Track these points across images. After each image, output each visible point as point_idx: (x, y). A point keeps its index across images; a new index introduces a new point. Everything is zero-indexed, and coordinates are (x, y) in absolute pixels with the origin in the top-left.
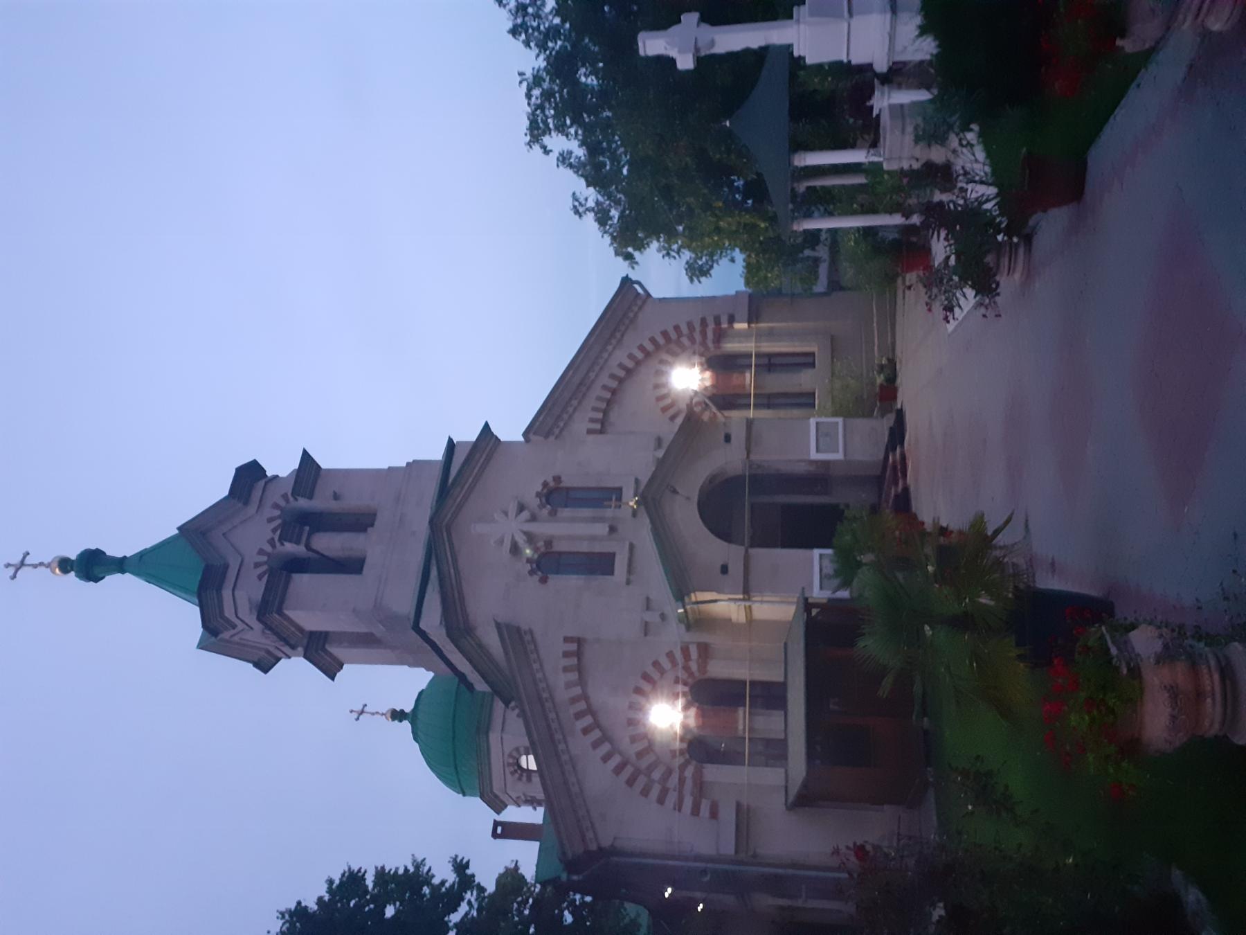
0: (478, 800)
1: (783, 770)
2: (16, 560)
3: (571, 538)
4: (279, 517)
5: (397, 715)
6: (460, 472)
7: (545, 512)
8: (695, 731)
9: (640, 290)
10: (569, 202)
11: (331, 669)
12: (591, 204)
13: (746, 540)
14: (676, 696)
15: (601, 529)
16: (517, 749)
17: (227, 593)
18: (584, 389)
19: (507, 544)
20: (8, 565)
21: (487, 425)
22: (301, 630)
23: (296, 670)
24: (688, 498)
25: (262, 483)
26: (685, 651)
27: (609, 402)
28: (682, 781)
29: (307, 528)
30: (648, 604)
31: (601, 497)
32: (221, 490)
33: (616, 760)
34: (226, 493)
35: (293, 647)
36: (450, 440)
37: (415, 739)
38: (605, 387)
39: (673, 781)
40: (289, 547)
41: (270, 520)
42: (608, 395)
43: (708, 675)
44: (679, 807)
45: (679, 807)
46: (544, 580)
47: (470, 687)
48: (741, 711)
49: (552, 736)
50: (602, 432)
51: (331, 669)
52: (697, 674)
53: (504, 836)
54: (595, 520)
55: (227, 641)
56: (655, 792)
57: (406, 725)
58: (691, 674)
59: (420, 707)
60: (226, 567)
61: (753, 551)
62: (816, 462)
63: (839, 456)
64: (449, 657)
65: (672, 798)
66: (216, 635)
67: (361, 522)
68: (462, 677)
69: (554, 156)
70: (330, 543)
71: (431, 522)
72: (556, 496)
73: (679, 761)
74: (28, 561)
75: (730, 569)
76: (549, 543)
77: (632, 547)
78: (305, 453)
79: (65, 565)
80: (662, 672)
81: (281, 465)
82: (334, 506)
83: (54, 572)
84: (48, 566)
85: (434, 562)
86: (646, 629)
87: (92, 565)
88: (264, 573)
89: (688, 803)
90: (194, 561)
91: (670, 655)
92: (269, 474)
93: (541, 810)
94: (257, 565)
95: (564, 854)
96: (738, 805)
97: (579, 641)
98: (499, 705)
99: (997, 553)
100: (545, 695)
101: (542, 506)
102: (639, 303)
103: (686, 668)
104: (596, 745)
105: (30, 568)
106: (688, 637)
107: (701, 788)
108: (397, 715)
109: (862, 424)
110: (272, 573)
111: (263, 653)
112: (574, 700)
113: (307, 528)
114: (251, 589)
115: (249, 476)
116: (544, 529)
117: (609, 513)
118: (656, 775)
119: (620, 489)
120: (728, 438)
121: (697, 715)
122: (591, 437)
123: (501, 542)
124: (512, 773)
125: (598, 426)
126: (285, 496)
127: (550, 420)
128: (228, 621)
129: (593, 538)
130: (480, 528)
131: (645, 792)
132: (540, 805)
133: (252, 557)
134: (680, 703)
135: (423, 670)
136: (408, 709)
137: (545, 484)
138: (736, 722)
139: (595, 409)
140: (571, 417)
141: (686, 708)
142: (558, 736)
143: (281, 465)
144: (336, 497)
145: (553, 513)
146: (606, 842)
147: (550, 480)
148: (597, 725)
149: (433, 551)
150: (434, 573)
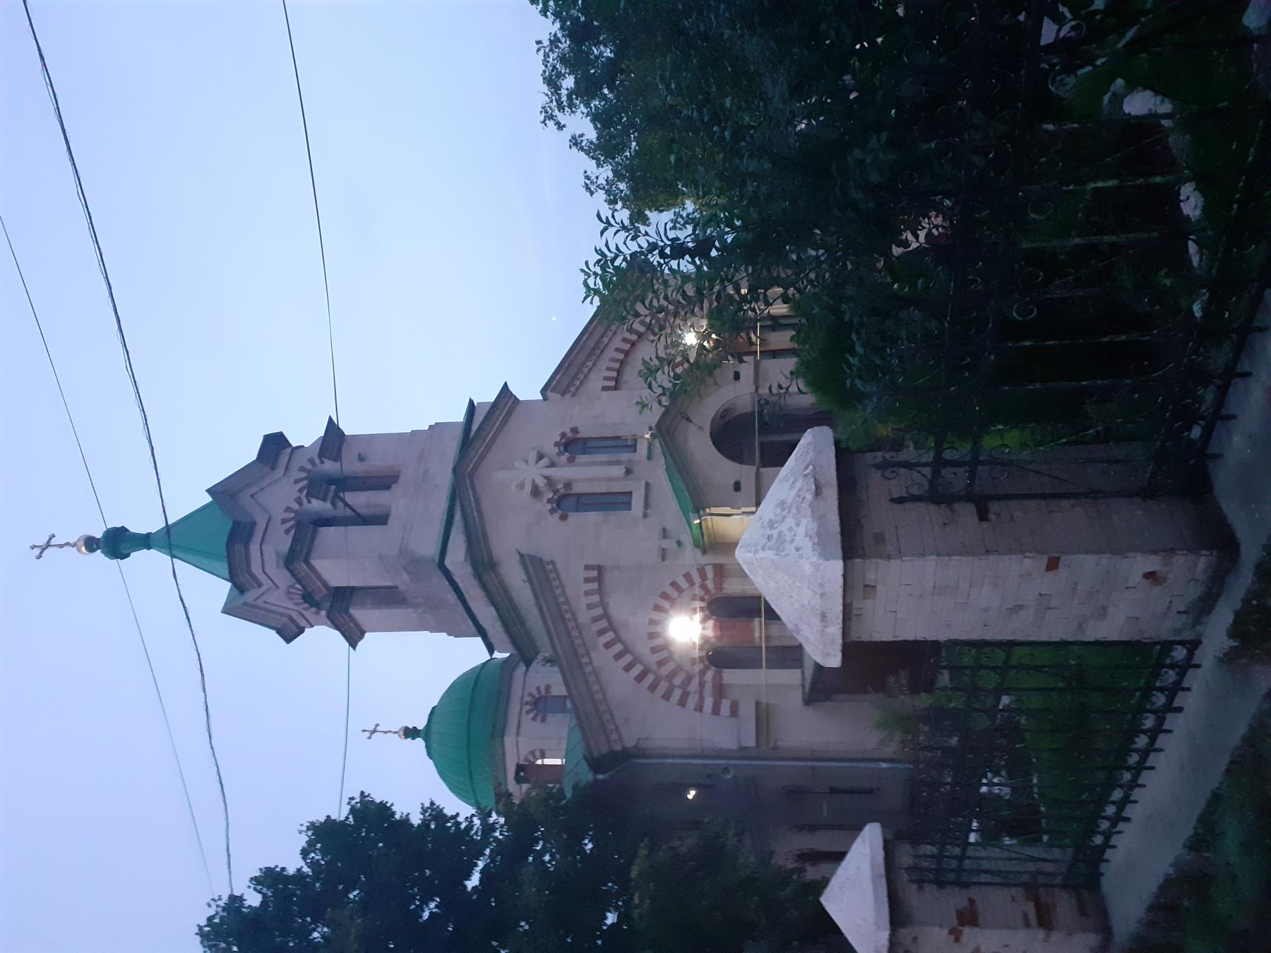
1: (799, 671)
2: (43, 542)
5: (410, 733)
6: (483, 423)
7: (564, 458)
8: (713, 640)
10: (582, 180)
11: (353, 636)
12: (602, 181)
13: (757, 459)
14: (694, 611)
15: (619, 471)
16: (533, 753)
17: (254, 548)
18: (598, 352)
19: (528, 488)
20: (33, 547)
21: (506, 384)
22: (325, 584)
23: (322, 638)
24: (701, 428)
25: (289, 450)
27: (622, 363)
28: (702, 684)
29: (333, 487)
30: (665, 534)
31: (621, 444)
32: (249, 453)
33: (638, 669)
34: (253, 456)
36: (471, 402)
37: (430, 754)
39: (696, 681)
41: (297, 482)
42: (621, 356)
44: (699, 708)
45: (699, 708)
46: (564, 518)
48: (756, 621)
49: (575, 651)
50: (616, 388)
52: (713, 591)
54: (611, 463)
56: (677, 694)
57: (420, 742)
58: (707, 591)
59: (434, 719)
60: (253, 525)
61: (763, 470)
65: (692, 701)
67: (385, 481)
69: (566, 135)
70: (359, 500)
71: (454, 470)
72: (573, 445)
73: (698, 667)
74: (53, 542)
76: (568, 485)
77: (647, 485)
79: (91, 544)
80: (680, 590)
81: (305, 434)
83: (79, 550)
84: (74, 545)
86: (664, 554)
87: (117, 543)
88: (291, 528)
89: (709, 702)
91: (688, 577)
94: (284, 521)
96: (758, 704)
97: (599, 569)
100: (568, 616)
101: (560, 454)
103: (703, 587)
104: (618, 657)
105: (55, 549)
106: (704, 560)
107: (720, 691)
108: (410, 733)
110: (299, 526)
111: (285, 619)
112: (596, 619)
115: (274, 445)
116: (563, 473)
118: (677, 681)
120: (737, 376)
121: (715, 626)
122: (606, 393)
123: (521, 486)
125: (613, 384)
126: (311, 461)
127: (566, 379)
129: (610, 479)
130: (502, 475)
131: (667, 696)
133: (279, 513)
134: (698, 617)
135: (445, 634)
136: (421, 726)
137: (563, 435)
138: (753, 630)
140: (586, 376)
141: (704, 621)
142: (581, 651)
143: (305, 434)
144: (361, 459)
146: (630, 742)
147: (567, 431)
148: (618, 639)
149: (455, 495)
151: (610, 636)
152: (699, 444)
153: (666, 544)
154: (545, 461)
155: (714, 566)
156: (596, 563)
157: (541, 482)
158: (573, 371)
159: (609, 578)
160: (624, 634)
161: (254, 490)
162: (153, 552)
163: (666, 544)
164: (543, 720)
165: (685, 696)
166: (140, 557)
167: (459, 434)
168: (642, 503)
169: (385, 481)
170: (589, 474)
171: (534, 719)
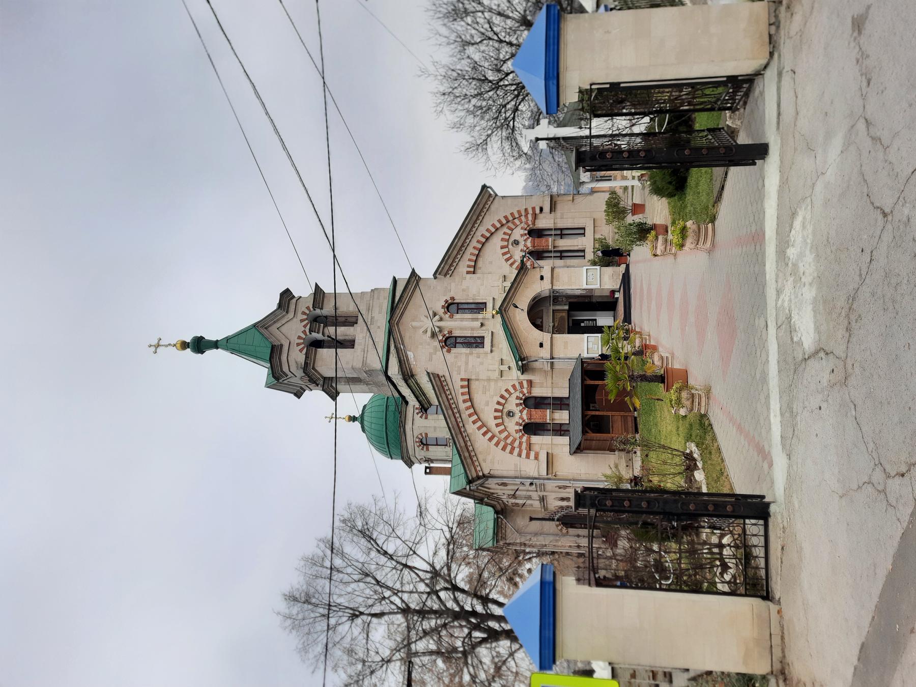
0: (401, 461)
2: (155, 342)
3: (461, 329)
5: (353, 419)
19: (429, 333)
20: (150, 346)
23: (316, 397)
25: (294, 301)
26: (521, 384)
27: (477, 256)
28: (521, 444)
33: (490, 435)
36: (394, 278)
38: (474, 248)
39: (516, 444)
41: (302, 321)
44: (520, 455)
45: (520, 455)
50: (474, 273)
53: (430, 473)
57: (357, 424)
60: (282, 345)
63: (598, 286)
65: (516, 451)
66: (277, 379)
67: (350, 321)
72: (453, 307)
77: (492, 333)
79: (184, 345)
81: (303, 291)
87: (199, 345)
88: (303, 348)
90: (257, 343)
94: (298, 344)
95: (468, 477)
99: (528, 166)
102: (491, 199)
108: (353, 419)
109: (609, 270)
112: (467, 408)
117: (480, 316)
118: (509, 441)
123: (426, 332)
125: (472, 269)
126: (308, 308)
128: (284, 373)
129: (473, 329)
137: (446, 301)
139: (470, 260)
143: (303, 291)
145: (451, 317)
148: (479, 419)
149: (390, 333)
151: (475, 417)
152: (521, 319)
153: (502, 368)
154: (437, 317)
156: (467, 377)
158: (450, 261)
159: (474, 385)
160: (481, 416)
161: (278, 325)
162: (220, 351)
163: (502, 368)
164: (426, 418)
166: (210, 353)
169: (350, 321)
170: (462, 325)
171: (421, 417)
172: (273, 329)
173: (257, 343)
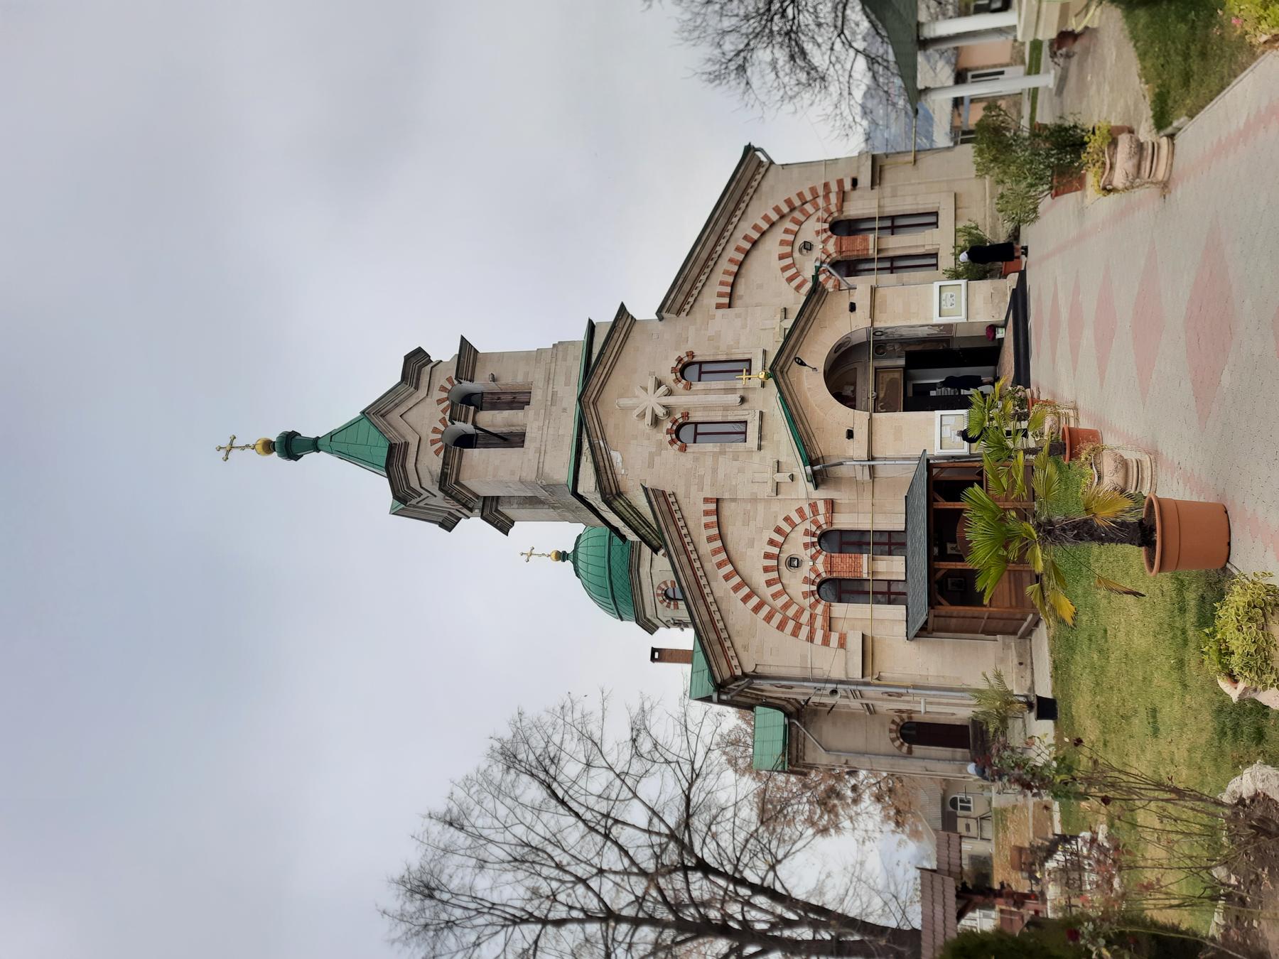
3: (706, 408)
4: (448, 399)
5: (562, 556)
9: (763, 159)
18: (711, 263)
21: (622, 305)
23: (473, 527)
26: (814, 506)
27: (736, 275)
30: (778, 466)
33: (754, 601)
34: (399, 380)
35: (471, 510)
36: (590, 321)
39: (805, 618)
40: (460, 425)
41: (440, 402)
43: (836, 527)
44: (811, 639)
45: (811, 639)
46: (683, 449)
47: (623, 538)
48: (865, 556)
49: (698, 583)
50: (730, 306)
51: (504, 526)
55: (414, 506)
57: (569, 564)
60: (407, 444)
61: (875, 415)
62: (939, 326)
63: (961, 318)
64: (604, 514)
65: (805, 631)
67: (518, 400)
68: (615, 530)
70: (493, 420)
71: (579, 399)
72: (688, 368)
74: (236, 443)
75: (844, 434)
77: (761, 414)
78: (464, 341)
79: (269, 447)
81: (444, 352)
82: (493, 387)
85: (585, 435)
88: (440, 448)
90: (376, 440)
92: (434, 359)
93: (690, 632)
94: (433, 442)
98: (646, 550)
102: (762, 170)
108: (562, 556)
112: (715, 552)
113: (472, 408)
114: (430, 462)
115: (416, 362)
116: (682, 400)
117: (740, 384)
118: (791, 612)
119: (749, 361)
122: (721, 311)
124: (661, 602)
128: (414, 490)
129: (726, 408)
132: (687, 626)
133: (429, 436)
137: (680, 360)
143: (444, 352)
144: (494, 379)
145: (688, 387)
147: (683, 355)
149: (582, 423)
150: (586, 445)
154: (663, 389)
155: (826, 500)
157: (660, 412)
158: (687, 287)
159: (727, 510)
160: (740, 566)
161: (402, 409)
162: (322, 455)
165: (798, 626)
167: (580, 353)
168: (756, 435)
169: (518, 400)
170: (704, 400)
172: (394, 417)
173: (376, 440)
